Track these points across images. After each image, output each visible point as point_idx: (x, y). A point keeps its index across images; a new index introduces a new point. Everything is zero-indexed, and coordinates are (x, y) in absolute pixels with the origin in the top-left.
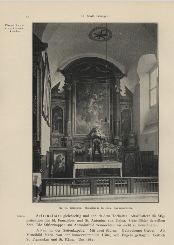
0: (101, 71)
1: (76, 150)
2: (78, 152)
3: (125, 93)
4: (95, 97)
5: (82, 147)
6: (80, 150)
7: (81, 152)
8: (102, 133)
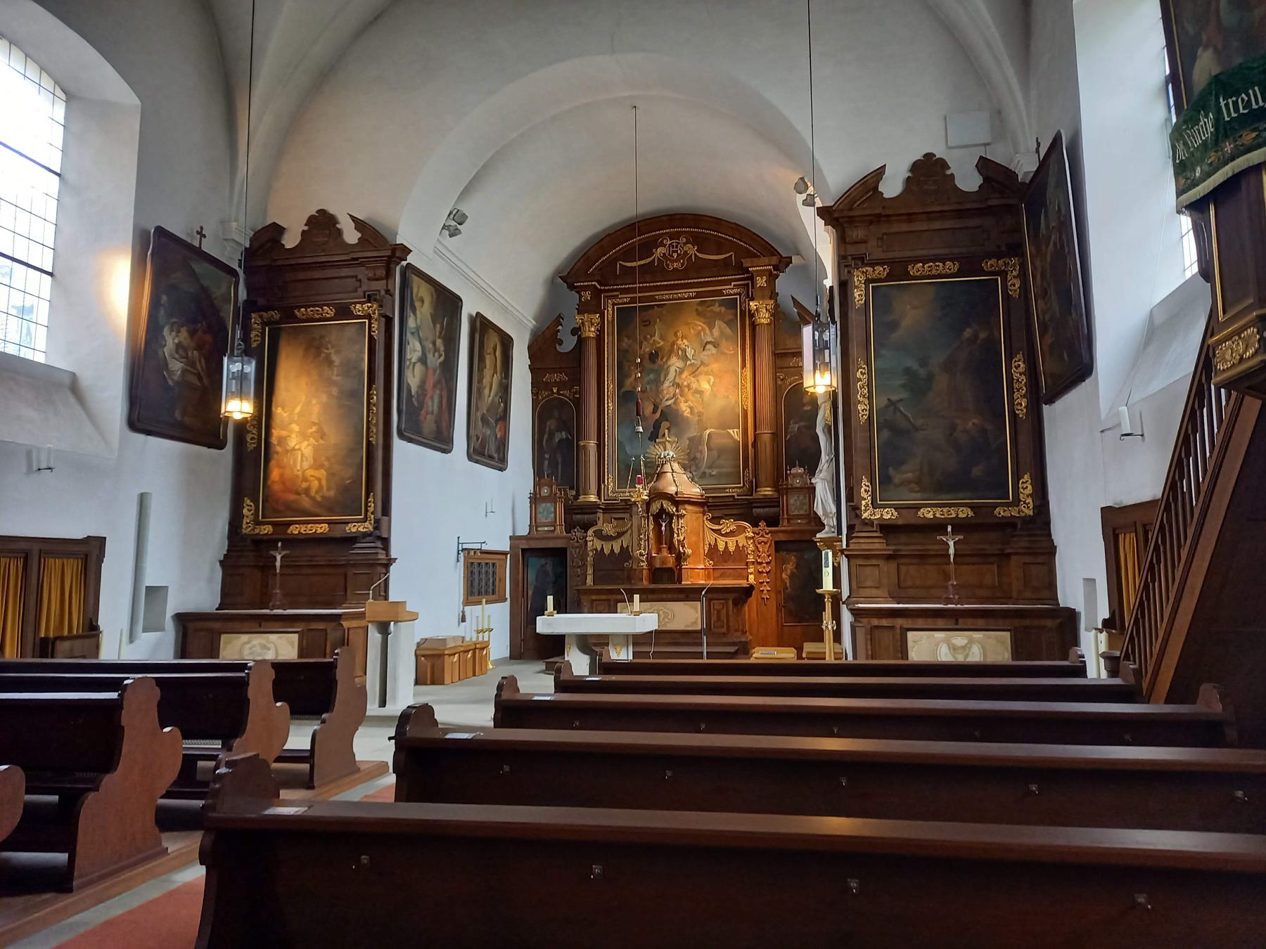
1: (598, 544)
2: (607, 551)
5: (620, 535)
7: (732, 548)
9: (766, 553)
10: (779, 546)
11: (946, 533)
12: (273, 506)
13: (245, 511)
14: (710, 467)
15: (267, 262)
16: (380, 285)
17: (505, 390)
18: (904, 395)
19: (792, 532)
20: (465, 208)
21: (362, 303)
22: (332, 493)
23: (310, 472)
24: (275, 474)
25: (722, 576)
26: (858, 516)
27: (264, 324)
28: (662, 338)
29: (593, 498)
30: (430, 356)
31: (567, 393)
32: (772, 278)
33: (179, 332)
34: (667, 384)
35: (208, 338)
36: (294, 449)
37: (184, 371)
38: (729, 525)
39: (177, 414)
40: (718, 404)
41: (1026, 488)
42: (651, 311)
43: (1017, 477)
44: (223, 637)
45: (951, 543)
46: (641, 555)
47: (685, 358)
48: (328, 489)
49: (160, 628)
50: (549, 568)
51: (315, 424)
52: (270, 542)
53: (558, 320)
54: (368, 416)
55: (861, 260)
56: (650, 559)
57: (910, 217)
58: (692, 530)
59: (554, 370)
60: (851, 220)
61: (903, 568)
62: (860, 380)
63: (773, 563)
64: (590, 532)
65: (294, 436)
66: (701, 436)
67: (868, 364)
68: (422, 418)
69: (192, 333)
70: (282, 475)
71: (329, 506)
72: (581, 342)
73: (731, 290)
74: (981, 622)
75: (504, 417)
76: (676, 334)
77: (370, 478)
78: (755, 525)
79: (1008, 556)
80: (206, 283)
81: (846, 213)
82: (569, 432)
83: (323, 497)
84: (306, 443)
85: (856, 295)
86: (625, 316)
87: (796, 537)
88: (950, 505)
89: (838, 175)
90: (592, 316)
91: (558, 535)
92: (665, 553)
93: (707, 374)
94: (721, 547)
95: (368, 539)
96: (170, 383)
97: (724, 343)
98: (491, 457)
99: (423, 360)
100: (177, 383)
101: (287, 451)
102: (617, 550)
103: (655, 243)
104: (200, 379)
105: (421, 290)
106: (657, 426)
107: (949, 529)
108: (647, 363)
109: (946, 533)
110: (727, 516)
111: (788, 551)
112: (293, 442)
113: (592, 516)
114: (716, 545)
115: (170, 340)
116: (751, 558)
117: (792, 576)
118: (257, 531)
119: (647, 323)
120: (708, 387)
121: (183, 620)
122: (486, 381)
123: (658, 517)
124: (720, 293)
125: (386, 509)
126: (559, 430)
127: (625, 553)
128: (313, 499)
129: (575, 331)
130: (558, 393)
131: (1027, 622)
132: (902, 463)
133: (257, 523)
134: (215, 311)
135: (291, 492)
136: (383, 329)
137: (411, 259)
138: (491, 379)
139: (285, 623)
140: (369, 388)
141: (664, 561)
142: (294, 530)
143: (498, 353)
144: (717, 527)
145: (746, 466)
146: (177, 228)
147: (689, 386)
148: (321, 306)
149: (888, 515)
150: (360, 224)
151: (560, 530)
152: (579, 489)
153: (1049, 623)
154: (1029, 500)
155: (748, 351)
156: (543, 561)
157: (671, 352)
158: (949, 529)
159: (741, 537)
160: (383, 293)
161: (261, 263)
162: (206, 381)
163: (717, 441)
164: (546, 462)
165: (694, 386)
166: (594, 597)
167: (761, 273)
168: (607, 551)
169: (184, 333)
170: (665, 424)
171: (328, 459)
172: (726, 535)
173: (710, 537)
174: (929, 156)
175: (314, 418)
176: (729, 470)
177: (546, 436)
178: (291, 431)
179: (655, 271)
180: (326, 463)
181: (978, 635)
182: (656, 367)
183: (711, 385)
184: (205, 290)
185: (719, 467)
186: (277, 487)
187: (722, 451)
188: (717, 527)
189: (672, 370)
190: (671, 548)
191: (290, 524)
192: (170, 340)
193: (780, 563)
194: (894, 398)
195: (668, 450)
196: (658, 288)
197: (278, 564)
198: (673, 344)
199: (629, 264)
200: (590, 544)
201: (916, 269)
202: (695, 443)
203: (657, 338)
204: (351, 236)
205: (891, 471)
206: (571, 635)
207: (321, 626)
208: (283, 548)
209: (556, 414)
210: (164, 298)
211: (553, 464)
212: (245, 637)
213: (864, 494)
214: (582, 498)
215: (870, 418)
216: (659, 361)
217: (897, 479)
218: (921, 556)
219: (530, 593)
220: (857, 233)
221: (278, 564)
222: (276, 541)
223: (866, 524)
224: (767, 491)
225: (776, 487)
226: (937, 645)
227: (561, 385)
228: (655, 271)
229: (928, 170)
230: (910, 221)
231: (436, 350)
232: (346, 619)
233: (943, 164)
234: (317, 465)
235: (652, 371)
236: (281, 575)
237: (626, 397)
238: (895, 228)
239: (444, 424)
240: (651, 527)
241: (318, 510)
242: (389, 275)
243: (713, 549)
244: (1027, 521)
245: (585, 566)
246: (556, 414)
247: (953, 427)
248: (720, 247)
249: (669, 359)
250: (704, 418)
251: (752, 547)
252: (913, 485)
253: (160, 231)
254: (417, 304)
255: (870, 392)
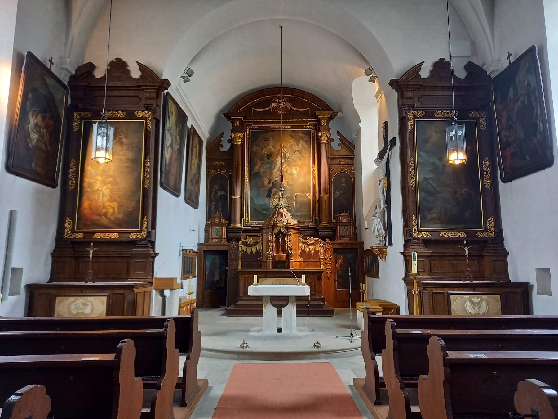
0: (293, 108)
1: (244, 248)
2: (249, 252)
3: (339, 145)
4: (284, 154)
5: (256, 244)
6: (253, 248)
7: (254, 252)
8: (341, 264)
9: (329, 252)
10: (336, 251)
11: (464, 245)
12: (83, 221)
13: (67, 225)
14: (297, 212)
15: (85, 84)
16: (153, 102)
17: (199, 166)
18: (432, 176)
19: (342, 244)
20: (193, 68)
21: (143, 111)
22: (121, 216)
23: (108, 204)
24: (86, 204)
25: (307, 265)
26: (411, 235)
27: (81, 119)
28: (273, 147)
29: (238, 225)
30: (174, 144)
31: (225, 171)
32: (328, 121)
33: (37, 116)
34: (276, 170)
35: (51, 122)
36: (98, 190)
37: (38, 140)
38: (311, 240)
39: (33, 165)
40: (301, 180)
41: (491, 223)
42: (268, 134)
43: (486, 218)
44: (58, 299)
45: (466, 250)
46: (269, 254)
47: (285, 158)
48: (119, 214)
49: (18, 294)
50: (217, 260)
51: (112, 176)
52: (85, 243)
53: (222, 135)
54: (144, 173)
55: (412, 107)
56: (273, 256)
57: (435, 88)
58: (294, 241)
59: (218, 160)
60: (408, 87)
61: (432, 262)
62: (411, 167)
63: (332, 259)
64: (240, 242)
65: (98, 182)
66: (292, 197)
67: (414, 159)
68: (170, 177)
69: (44, 118)
70: (90, 205)
71: (119, 224)
72: (233, 147)
73: (308, 126)
74: (486, 290)
75: (198, 182)
76: (280, 146)
77: (144, 208)
78: (324, 240)
79: (483, 256)
80: (52, 91)
81: (405, 83)
82: (225, 191)
83: (115, 218)
84: (105, 187)
85: (409, 124)
86: (255, 135)
87: (344, 246)
88: (455, 231)
89: (398, 66)
90: (240, 134)
91: (224, 245)
92: (281, 254)
93: (296, 166)
94: (307, 251)
95: (143, 242)
96: (30, 146)
97: (304, 151)
98: (193, 202)
99: (171, 145)
100: (34, 146)
101: (94, 191)
102: (254, 252)
103: (271, 101)
104: (46, 146)
105: (172, 108)
106: (270, 190)
107: (465, 242)
108: (266, 159)
109: (464, 245)
110: (310, 236)
111: (340, 253)
112: (97, 186)
113: (238, 234)
114: (304, 250)
115: (32, 121)
116: (322, 257)
117: (341, 266)
118: (74, 236)
119: (266, 139)
120: (296, 172)
121: (31, 289)
122: (193, 161)
123: (277, 235)
124: (302, 127)
125: (154, 226)
126: (220, 190)
127: (258, 253)
128: (109, 219)
129: (229, 141)
130: (220, 171)
131: (508, 290)
132: (431, 209)
133: (73, 231)
134: (56, 108)
135: (96, 214)
136: (154, 126)
137: (170, 90)
138: (195, 161)
139: (97, 290)
140: (145, 158)
141: (280, 257)
142: (97, 236)
143: (198, 148)
144: (305, 241)
145: (314, 211)
146: (38, 55)
147: (286, 171)
148: (118, 111)
149: (426, 235)
150: (142, 68)
151: (224, 241)
152: (231, 220)
153: (518, 290)
154: (493, 229)
155: (316, 154)
156: (214, 256)
157: (278, 154)
158: (465, 242)
159: (317, 246)
160: (155, 106)
161: (82, 84)
162: (49, 148)
163: (299, 199)
164: (213, 206)
165: (289, 171)
166: (246, 276)
167: (324, 119)
168: (249, 252)
169: (39, 118)
170: (274, 190)
171: (119, 197)
172: (310, 245)
173: (302, 246)
174: (442, 60)
175: (111, 173)
176: (306, 213)
177: (213, 193)
178: (97, 180)
179: (272, 114)
180: (118, 199)
181: (485, 297)
182: (270, 161)
183: (298, 171)
184: (51, 95)
185: (300, 212)
186: (86, 212)
187: (302, 204)
188: (305, 241)
189: (279, 163)
190: (284, 251)
191: (94, 233)
192: (32, 121)
193: (336, 259)
194: (427, 177)
195: (277, 201)
196: (272, 123)
197: (91, 255)
198: (279, 150)
199: (258, 110)
200: (240, 248)
201: (438, 114)
202: (289, 198)
203: (271, 147)
204: (136, 74)
205: (426, 213)
206: (267, 297)
207: (121, 292)
208: (94, 246)
209: (219, 182)
210: (30, 95)
211: (217, 208)
212: (72, 299)
213: (414, 224)
214: (233, 225)
215: (416, 187)
216: (272, 159)
217: (429, 217)
218: (442, 256)
219: (207, 273)
220: (408, 94)
221: (91, 255)
222: (90, 242)
223: (416, 239)
224: (325, 224)
225: (330, 222)
226: (465, 302)
227: (222, 168)
228: (272, 114)
229: (441, 66)
230: (434, 90)
231: (176, 142)
232: (137, 288)
233: (449, 64)
234: (112, 200)
235: (268, 163)
236: (93, 262)
237: (255, 176)
238: (427, 93)
239: (178, 182)
240: (274, 240)
241: (112, 225)
242: (158, 96)
243: (303, 251)
244: (493, 239)
245: (237, 260)
246: (219, 182)
247: (456, 192)
248: (302, 105)
249: (277, 157)
250: (294, 187)
251: (322, 251)
252: (437, 220)
253: (30, 54)
254: (170, 115)
255: (415, 173)
